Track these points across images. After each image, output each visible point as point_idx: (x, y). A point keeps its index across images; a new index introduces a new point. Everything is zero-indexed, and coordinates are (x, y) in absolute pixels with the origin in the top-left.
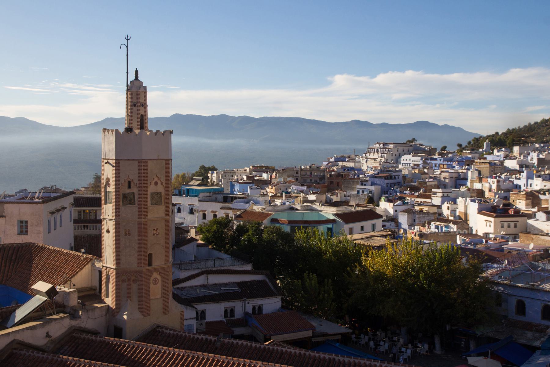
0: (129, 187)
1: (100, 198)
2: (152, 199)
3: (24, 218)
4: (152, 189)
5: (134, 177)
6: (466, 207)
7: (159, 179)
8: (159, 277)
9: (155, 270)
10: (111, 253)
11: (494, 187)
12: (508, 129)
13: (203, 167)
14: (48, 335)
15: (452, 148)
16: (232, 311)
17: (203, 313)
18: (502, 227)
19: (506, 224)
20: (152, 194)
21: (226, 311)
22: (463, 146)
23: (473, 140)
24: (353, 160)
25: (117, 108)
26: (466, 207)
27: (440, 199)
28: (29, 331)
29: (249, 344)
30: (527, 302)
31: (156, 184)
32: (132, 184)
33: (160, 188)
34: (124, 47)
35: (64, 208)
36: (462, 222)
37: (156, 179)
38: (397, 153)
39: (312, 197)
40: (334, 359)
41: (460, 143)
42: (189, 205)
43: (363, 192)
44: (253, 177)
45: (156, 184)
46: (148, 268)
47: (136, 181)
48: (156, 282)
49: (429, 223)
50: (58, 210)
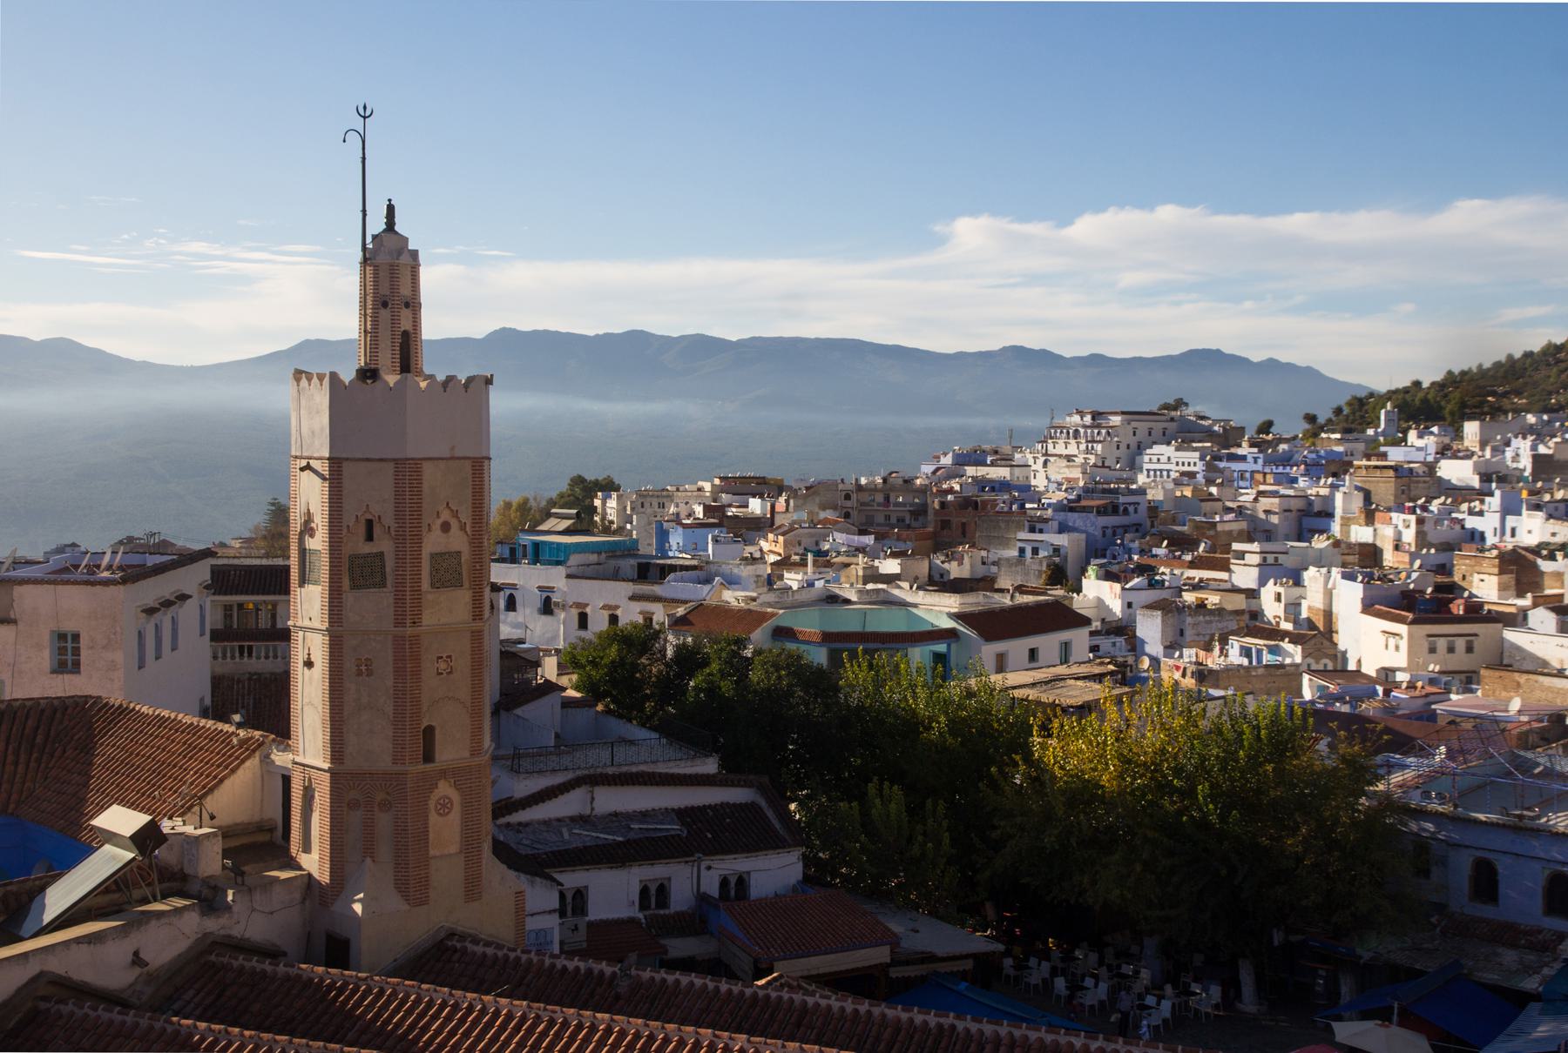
0: (370, 537)
2: (435, 570)
3: (69, 626)
4: (434, 542)
5: (384, 509)
6: (1329, 595)
7: (455, 514)
8: (455, 796)
9: (443, 774)
10: (318, 724)
11: (1409, 536)
13: (578, 481)
14: (137, 960)
15: (1290, 426)
16: (663, 891)
17: (580, 895)
18: (1432, 650)
19: (1442, 643)
20: (433, 556)
21: (644, 892)
22: (1321, 420)
23: (1349, 404)
24: (1005, 460)
26: (1329, 595)
27: (1255, 572)
28: (84, 947)
29: (711, 985)
30: (1503, 866)
31: (446, 527)
32: (377, 530)
33: (457, 541)
34: (355, 140)
35: (183, 597)
36: (1318, 636)
37: (446, 516)
38: (1133, 441)
39: (891, 566)
40: (953, 1027)
41: (1312, 411)
42: (541, 588)
43: (1035, 551)
44: (722, 509)
45: (446, 527)
46: (422, 767)
47: (389, 520)
48: (445, 807)
49: (1224, 641)
50: (167, 604)
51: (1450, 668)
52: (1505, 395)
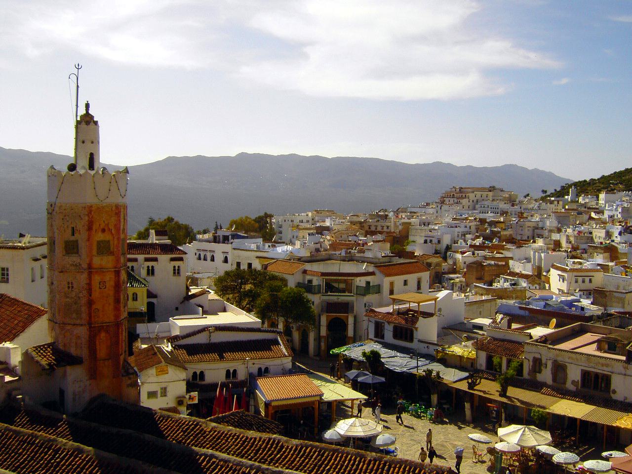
1: (156, 235)
12: (170, 220)
13: (266, 214)
18: (576, 282)
19: (580, 279)
21: (228, 372)
22: (548, 193)
25: (63, 145)
34: (74, 78)
38: (475, 199)
51: (582, 289)
52: (617, 184)
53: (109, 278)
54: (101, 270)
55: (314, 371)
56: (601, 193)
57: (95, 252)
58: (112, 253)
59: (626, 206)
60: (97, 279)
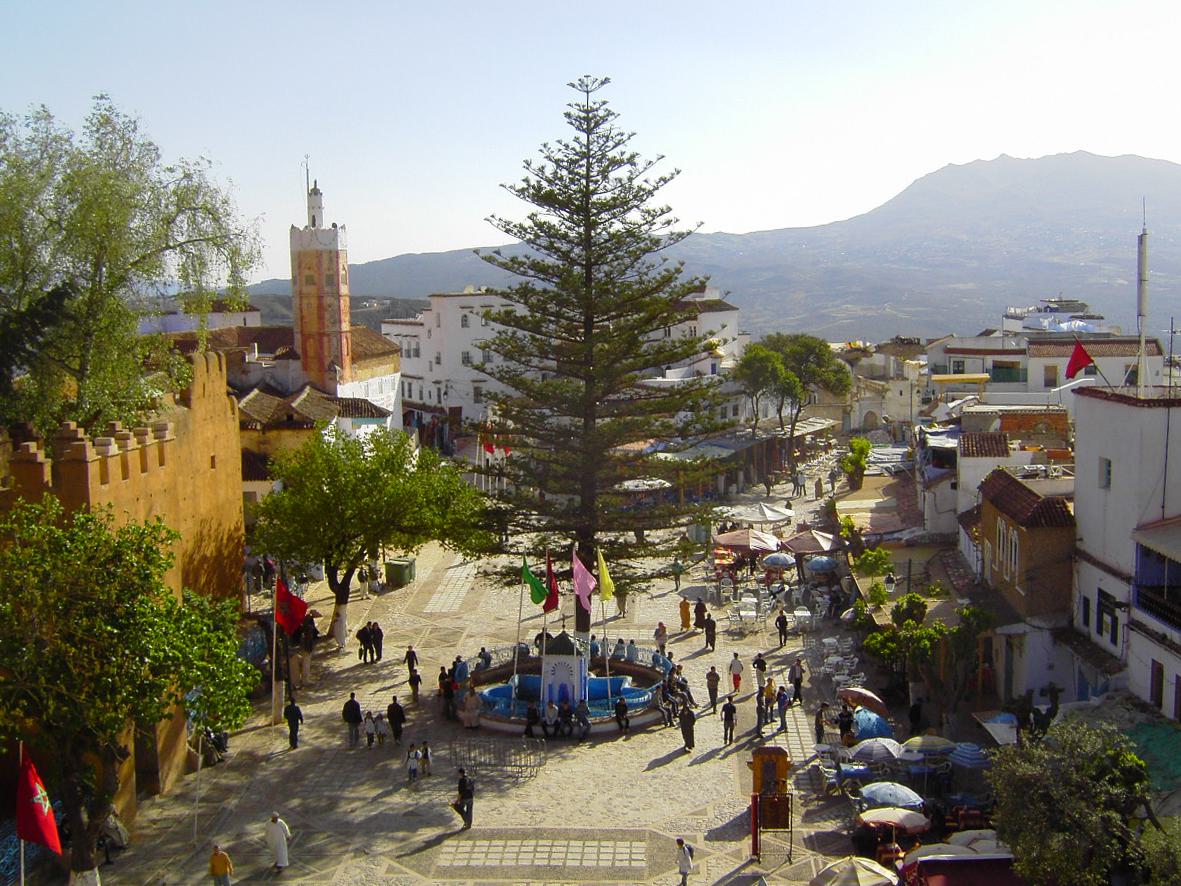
53: (314, 301)
54: (308, 296)
55: (872, 698)
56: (1020, 696)
57: (304, 283)
58: (314, 284)
59: (883, 618)
60: (305, 301)
